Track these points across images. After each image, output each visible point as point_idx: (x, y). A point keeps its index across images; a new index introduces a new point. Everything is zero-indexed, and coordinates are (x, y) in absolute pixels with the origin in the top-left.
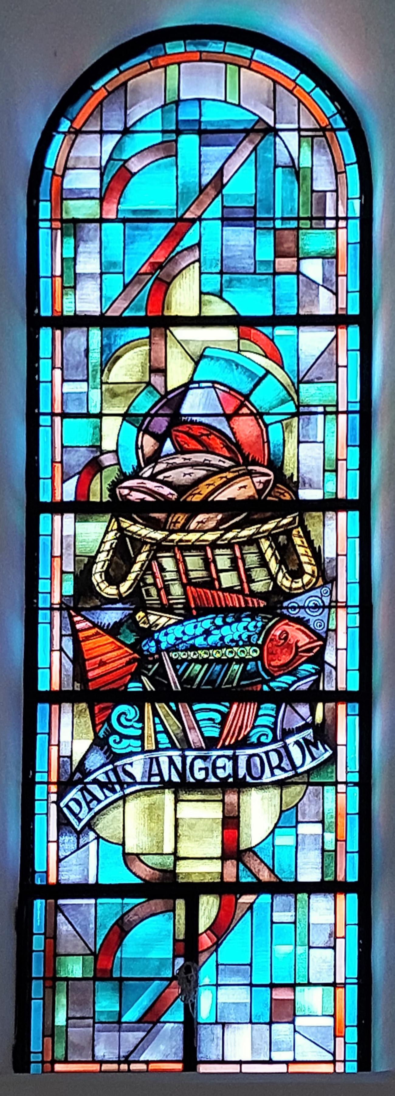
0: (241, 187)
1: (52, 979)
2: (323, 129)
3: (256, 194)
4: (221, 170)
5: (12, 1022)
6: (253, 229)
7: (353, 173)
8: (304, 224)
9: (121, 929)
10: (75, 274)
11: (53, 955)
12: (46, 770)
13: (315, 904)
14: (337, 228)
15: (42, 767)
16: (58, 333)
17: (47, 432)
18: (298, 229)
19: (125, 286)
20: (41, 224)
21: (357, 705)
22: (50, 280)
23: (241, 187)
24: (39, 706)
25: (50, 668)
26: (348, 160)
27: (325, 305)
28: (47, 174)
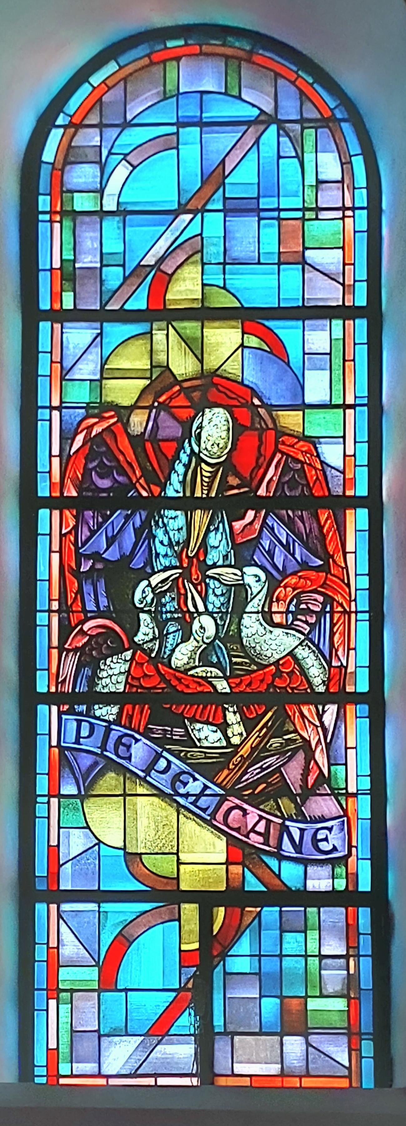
0: (243, 178)
1: (54, 991)
2: (328, 119)
3: (259, 184)
4: (223, 161)
5: (20, 363)
6: (257, 219)
7: (359, 164)
8: (309, 215)
9: (122, 943)
10: (72, 1003)
11: (55, 963)
12: (47, 578)
13: (310, 337)
14: (343, 218)
15: (45, 265)
16: (57, 326)
17: (46, 228)
18: (303, 219)
19: (125, 279)
20: (41, 217)
21: (366, 707)
22: (49, 273)
23: (243, 178)
24: (41, 324)
25: (48, 818)
26: (359, 339)
27: (331, 294)
28: (45, 172)
